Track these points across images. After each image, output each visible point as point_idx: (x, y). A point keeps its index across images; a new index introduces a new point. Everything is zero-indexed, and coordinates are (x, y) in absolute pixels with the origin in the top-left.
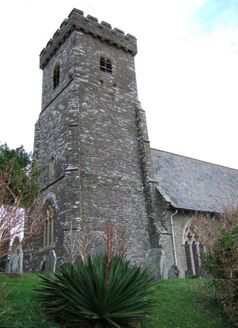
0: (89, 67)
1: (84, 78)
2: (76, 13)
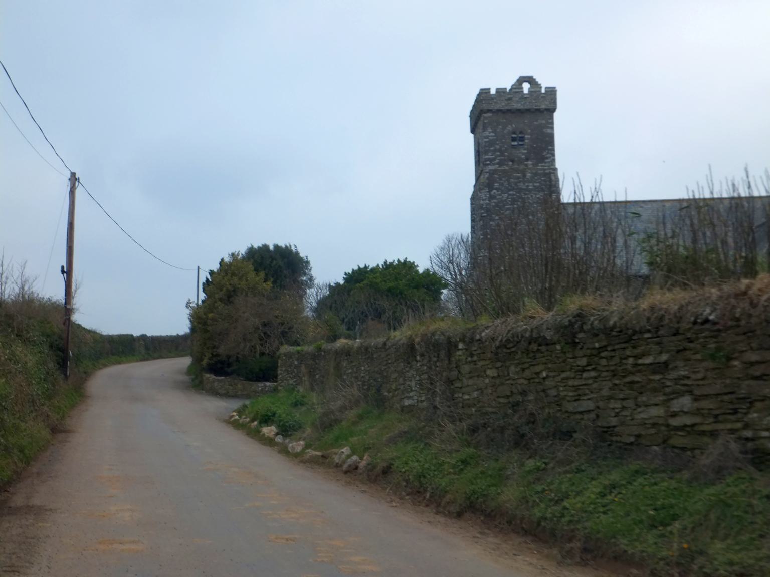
0: (500, 150)
1: (494, 164)
2: (483, 95)
